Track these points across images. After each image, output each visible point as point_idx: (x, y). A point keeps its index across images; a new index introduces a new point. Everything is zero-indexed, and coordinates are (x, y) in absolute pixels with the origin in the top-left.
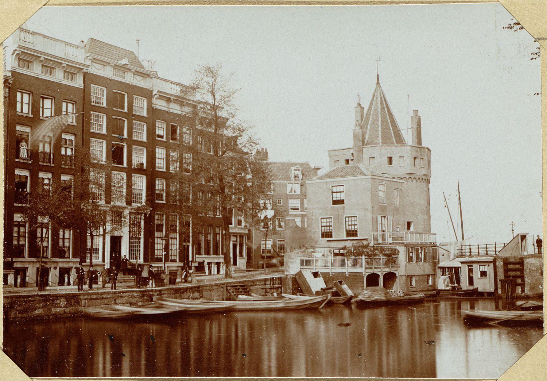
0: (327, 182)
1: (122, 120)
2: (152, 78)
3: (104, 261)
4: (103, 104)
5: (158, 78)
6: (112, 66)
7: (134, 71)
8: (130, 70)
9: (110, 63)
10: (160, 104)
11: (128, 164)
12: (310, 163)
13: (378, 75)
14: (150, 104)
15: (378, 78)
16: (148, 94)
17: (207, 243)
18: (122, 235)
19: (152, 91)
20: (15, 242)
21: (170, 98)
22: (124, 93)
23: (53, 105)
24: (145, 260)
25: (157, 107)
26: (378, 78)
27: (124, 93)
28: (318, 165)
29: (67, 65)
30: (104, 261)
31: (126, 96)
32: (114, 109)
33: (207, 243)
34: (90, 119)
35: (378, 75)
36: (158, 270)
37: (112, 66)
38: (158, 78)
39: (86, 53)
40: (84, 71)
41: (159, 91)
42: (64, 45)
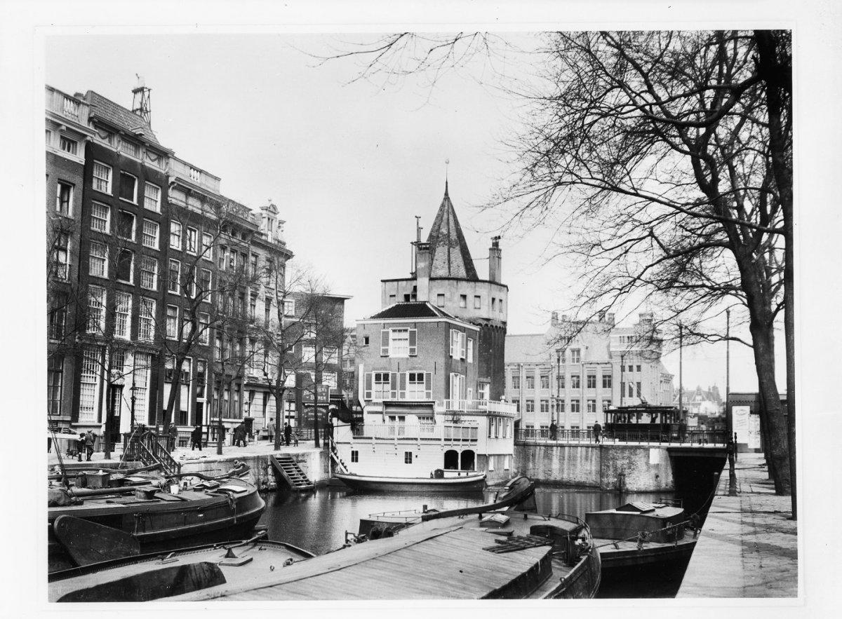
0: (415, 323)
3: (100, 421)
4: (101, 189)
5: (175, 159)
10: (176, 197)
11: (138, 202)
13: (447, 183)
14: (165, 197)
15: (447, 187)
16: (162, 183)
18: (124, 383)
20: (313, 430)
21: (190, 190)
22: (133, 215)
23: (166, 503)
25: (174, 201)
26: (447, 187)
27: (133, 215)
29: (67, 128)
30: (100, 421)
32: (120, 198)
35: (447, 183)
40: (88, 138)
42: (61, 97)
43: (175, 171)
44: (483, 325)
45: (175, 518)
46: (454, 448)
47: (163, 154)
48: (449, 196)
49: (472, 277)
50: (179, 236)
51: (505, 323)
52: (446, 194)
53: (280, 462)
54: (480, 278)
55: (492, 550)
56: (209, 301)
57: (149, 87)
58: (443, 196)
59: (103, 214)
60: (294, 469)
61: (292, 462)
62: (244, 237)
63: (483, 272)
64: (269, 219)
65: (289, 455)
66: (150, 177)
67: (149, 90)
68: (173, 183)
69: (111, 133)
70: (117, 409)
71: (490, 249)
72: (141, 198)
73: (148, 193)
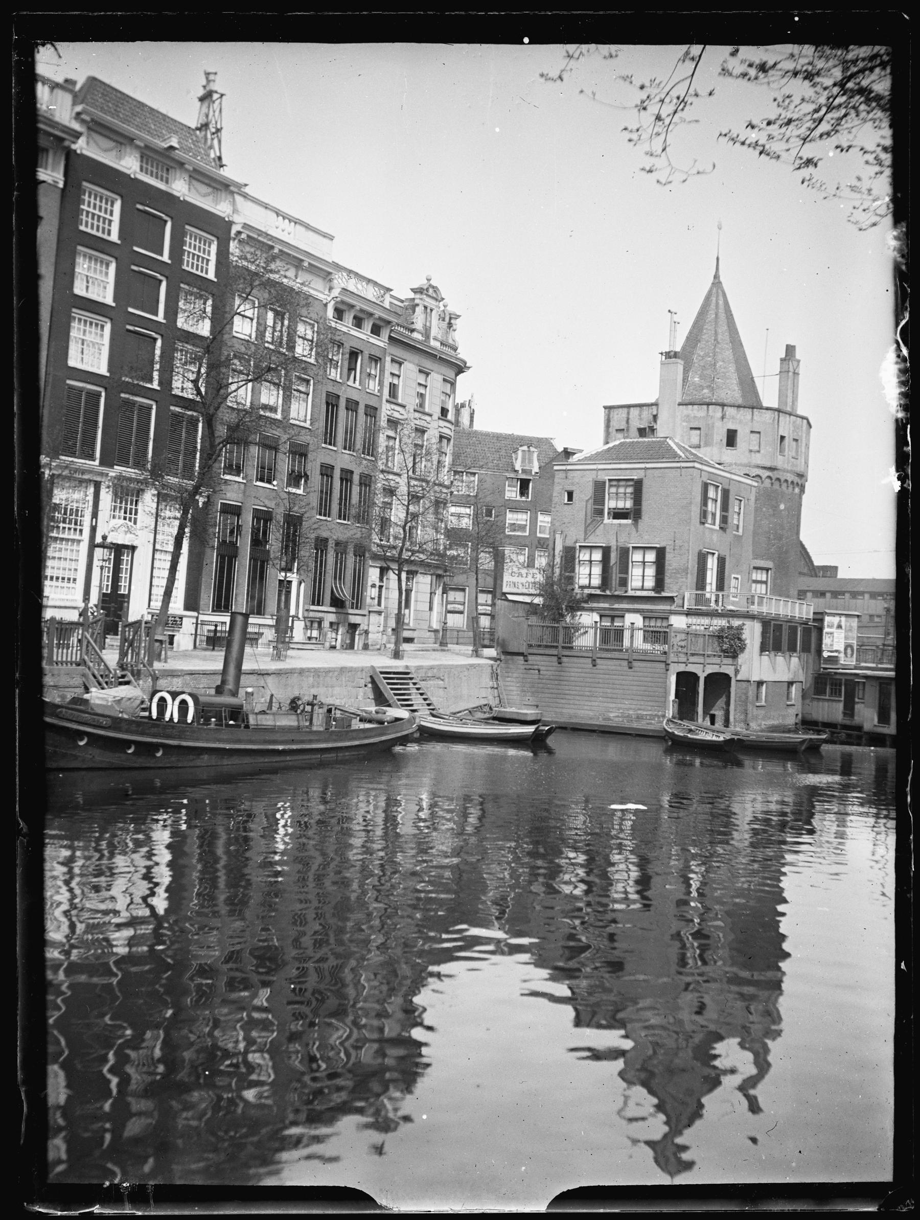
1: (160, 218)
2: (232, 193)
4: (109, 234)
5: (245, 196)
6: (138, 147)
7: (191, 168)
8: (181, 164)
9: (133, 140)
12: (554, 442)
13: (718, 259)
16: (219, 229)
17: (350, 432)
19: (231, 223)
24: (187, 607)
28: (571, 446)
29: (248, 236)
31: (159, 343)
33: (350, 432)
34: (80, 201)
35: (718, 259)
36: (215, 631)
37: (138, 147)
38: (245, 196)
39: (74, 104)
41: (246, 226)
43: (244, 215)
44: (764, 477)
45: (362, 735)
46: (691, 668)
47: (224, 187)
48: (722, 279)
49: (753, 403)
50: (252, 319)
51: (801, 476)
52: (716, 276)
53: (385, 678)
54: (765, 404)
55: (426, 1044)
56: (155, 385)
57: (221, 91)
58: (711, 279)
59: (101, 272)
60: (411, 686)
61: (411, 679)
62: (376, 330)
63: (769, 396)
64: (426, 307)
65: (407, 667)
66: (191, 217)
67: (222, 95)
68: (239, 233)
69: (121, 144)
70: (123, 583)
71: (782, 360)
72: (177, 251)
73: (190, 246)
